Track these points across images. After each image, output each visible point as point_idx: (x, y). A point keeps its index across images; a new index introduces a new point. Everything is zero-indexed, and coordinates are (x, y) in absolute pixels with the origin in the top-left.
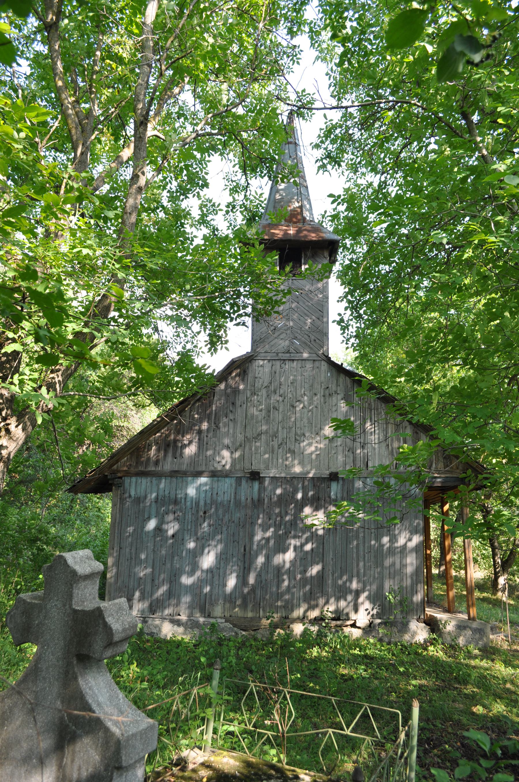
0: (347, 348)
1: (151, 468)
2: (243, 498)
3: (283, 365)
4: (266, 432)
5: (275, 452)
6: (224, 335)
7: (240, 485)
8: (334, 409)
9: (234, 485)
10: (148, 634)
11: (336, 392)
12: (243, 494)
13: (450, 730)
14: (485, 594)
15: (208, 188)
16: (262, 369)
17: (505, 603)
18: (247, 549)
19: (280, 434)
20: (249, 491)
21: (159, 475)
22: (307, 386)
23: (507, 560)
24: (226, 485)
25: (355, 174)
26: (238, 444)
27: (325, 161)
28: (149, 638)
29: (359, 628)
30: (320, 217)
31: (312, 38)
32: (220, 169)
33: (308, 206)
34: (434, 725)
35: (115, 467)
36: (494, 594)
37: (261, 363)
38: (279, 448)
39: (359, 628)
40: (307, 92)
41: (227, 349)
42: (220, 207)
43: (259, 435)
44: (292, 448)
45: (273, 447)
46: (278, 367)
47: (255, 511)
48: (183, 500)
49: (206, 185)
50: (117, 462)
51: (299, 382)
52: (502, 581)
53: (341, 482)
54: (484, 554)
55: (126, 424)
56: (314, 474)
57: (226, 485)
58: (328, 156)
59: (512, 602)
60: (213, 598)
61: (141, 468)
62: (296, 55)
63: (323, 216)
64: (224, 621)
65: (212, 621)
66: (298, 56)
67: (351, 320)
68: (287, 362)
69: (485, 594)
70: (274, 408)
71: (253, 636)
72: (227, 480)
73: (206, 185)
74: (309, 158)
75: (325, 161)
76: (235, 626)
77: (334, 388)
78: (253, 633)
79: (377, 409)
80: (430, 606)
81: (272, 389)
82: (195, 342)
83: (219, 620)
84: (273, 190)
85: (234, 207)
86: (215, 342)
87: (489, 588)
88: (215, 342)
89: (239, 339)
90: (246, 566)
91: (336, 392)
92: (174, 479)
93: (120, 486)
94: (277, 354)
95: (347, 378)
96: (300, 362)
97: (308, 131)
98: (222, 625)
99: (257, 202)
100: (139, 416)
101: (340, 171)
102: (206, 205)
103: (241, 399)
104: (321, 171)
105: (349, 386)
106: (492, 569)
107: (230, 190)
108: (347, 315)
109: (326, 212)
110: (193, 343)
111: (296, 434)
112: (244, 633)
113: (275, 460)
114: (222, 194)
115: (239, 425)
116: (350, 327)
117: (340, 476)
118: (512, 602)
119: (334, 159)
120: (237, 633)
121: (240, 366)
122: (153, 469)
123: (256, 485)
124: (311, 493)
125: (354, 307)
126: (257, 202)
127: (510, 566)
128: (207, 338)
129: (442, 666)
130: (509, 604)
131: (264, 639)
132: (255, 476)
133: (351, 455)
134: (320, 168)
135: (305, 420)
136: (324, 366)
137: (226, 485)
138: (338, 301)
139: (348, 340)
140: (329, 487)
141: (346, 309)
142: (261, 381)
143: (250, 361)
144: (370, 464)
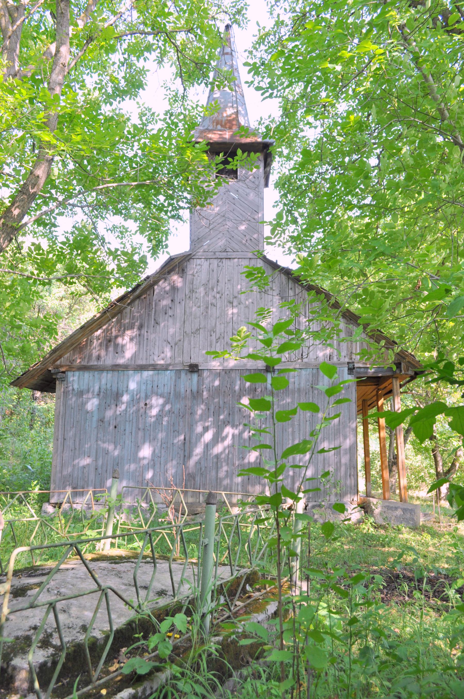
1: (94, 362)
2: (183, 391)
3: (220, 264)
7: (180, 378)
9: (174, 378)
12: (182, 386)
16: (199, 269)
24: (166, 378)
32: (160, 80)
35: (58, 362)
43: (198, 330)
45: (211, 342)
50: (60, 357)
68: (224, 260)
90: (186, 454)
92: (116, 373)
94: (215, 253)
105: (284, 283)
114: (159, 96)
115: (178, 320)
121: (176, 265)
122: (96, 363)
123: (195, 377)
132: (193, 368)
138: (274, 206)
143: (188, 260)
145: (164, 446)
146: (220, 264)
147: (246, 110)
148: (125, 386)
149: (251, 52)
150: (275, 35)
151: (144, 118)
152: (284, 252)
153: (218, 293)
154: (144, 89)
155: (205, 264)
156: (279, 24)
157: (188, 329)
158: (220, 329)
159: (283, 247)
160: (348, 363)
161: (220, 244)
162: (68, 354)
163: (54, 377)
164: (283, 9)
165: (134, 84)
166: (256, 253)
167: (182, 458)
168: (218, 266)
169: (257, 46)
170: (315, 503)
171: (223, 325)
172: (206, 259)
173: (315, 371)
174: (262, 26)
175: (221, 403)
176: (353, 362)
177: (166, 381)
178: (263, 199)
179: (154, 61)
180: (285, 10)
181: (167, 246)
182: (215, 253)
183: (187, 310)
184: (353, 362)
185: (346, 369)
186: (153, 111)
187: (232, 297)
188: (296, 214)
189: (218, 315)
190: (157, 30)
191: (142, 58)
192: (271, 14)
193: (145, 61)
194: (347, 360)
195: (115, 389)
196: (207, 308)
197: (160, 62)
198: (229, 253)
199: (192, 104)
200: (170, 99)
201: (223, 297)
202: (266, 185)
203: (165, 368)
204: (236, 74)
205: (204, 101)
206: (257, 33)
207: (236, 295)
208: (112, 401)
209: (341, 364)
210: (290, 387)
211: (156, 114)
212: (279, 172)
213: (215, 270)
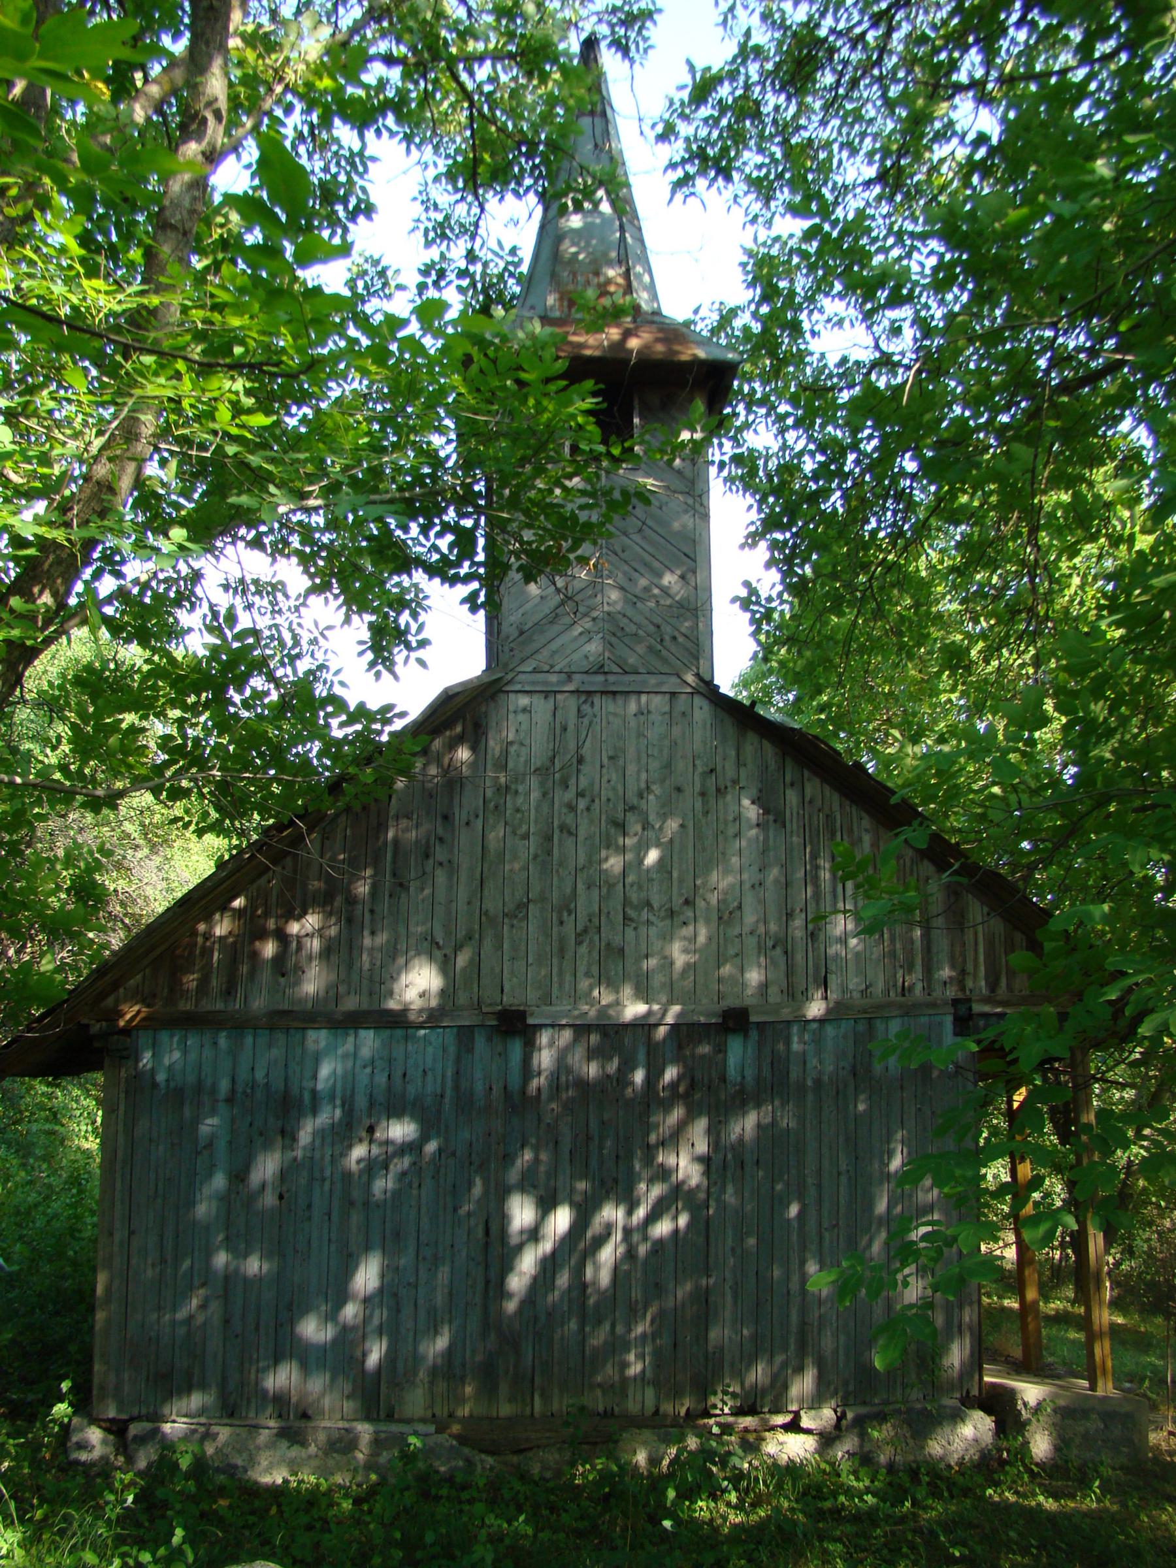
2: (479, 1087)
3: (586, 708)
4: (543, 899)
5: (569, 955)
6: (414, 627)
7: (471, 1050)
8: (731, 831)
9: (452, 1049)
12: (478, 1075)
15: (369, 217)
16: (523, 724)
18: (494, 1229)
19: (581, 901)
21: (239, 1025)
22: (654, 765)
25: (767, 204)
26: (461, 934)
27: (691, 169)
28: (221, 1478)
29: (808, 1431)
33: (646, 278)
37: (524, 701)
38: (579, 943)
39: (808, 1431)
41: (422, 663)
43: (523, 906)
44: (617, 940)
45: (562, 940)
46: (574, 710)
49: (366, 209)
51: (631, 752)
53: (754, 1035)
55: (122, 885)
58: (701, 155)
61: (185, 1006)
68: (597, 699)
70: (563, 828)
73: (366, 209)
74: (646, 165)
75: (691, 169)
77: (730, 773)
78: (515, 1459)
79: (851, 831)
81: (558, 771)
84: (549, 235)
85: (441, 274)
88: (386, 642)
89: (452, 642)
92: (281, 1037)
95: (766, 744)
100: (166, 862)
101: (728, 193)
103: (470, 801)
104: (679, 197)
105: (773, 765)
111: (626, 902)
112: (490, 1460)
113: (568, 977)
114: (407, 230)
117: (754, 1018)
119: (711, 162)
120: (469, 1462)
121: (459, 712)
122: (220, 1006)
123: (516, 1048)
124: (670, 1074)
128: (366, 635)
134: (679, 184)
136: (702, 711)
138: (742, 547)
140: (721, 1049)
142: (524, 751)
143: (493, 697)
144: (640, 505)
146: (586, 708)
151: (360, 284)
153: (580, 794)
155: (542, 708)
156: (747, 52)
157: (492, 904)
158: (586, 903)
160: (955, 1002)
162: (139, 977)
168: (580, 714)
170: (863, 1410)
173: (861, 1027)
175: (594, 1124)
176: (969, 1000)
178: (706, 517)
184: (969, 1000)
185: (948, 1020)
186: (383, 263)
187: (621, 807)
189: (582, 861)
194: (951, 992)
196: (549, 838)
198: (611, 678)
200: (427, 231)
204: (620, 171)
205: (525, 239)
207: (635, 801)
209: (934, 1005)
210: (793, 1076)
211: (389, 273)
213: (571, 727)
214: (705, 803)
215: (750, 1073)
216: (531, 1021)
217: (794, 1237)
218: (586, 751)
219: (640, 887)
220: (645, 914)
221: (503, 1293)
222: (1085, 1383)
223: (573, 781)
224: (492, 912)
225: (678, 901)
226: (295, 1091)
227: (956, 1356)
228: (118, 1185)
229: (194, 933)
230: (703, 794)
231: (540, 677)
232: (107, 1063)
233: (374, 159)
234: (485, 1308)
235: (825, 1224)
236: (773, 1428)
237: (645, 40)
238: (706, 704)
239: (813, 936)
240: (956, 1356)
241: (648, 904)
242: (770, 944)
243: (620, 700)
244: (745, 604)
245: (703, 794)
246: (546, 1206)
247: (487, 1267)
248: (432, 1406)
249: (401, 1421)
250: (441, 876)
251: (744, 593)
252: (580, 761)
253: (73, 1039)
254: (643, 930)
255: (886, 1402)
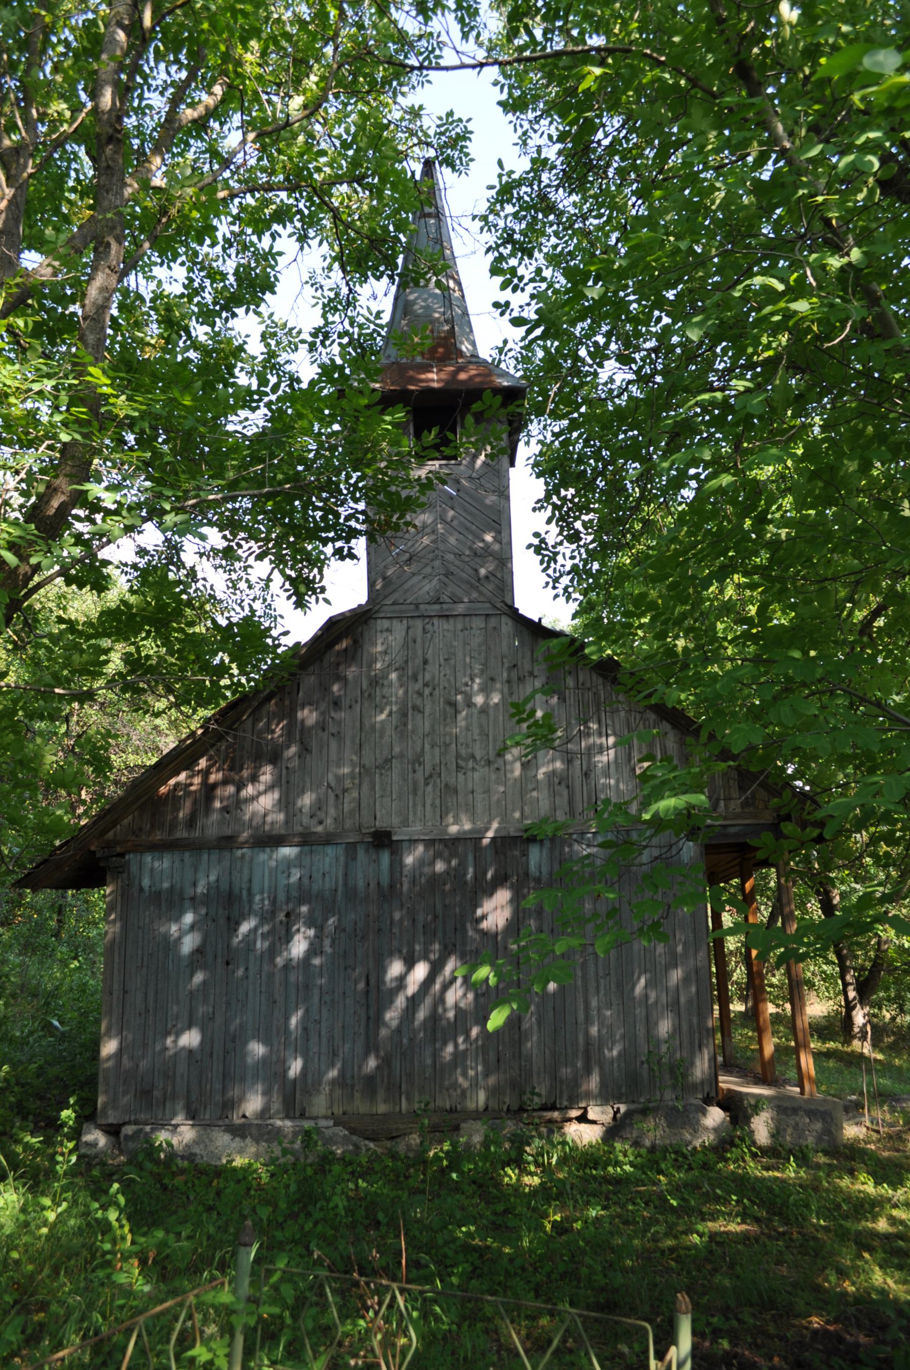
0: (556, 596)
1: (181, 833)
2: (361, 883)
4: (401, 755)
5: (420, 793)
7: (354, 859)
10: (183, 1157)
11: (531, 674)
12: (360, 875)
13: (772, 1329)
14: (831, 1045)
17: (868, 1059)
18: (372, 981)
19: (427, 757)
20: (371, 869)
21: (196, 847)
23: (867, 980)
24: (327, 860)
29: (594, 1122)
30: (495, 353)
31: (461, 21)
32: (303, 272)
34: (739, 1320)
35: (110, 835)
36: (848, 1041)
37: (386, 624)
38: (427, 784)
39: (594, 1122)
40: (456, 117)
41: (327, 601)
42: (302, 337)
43: (388, 761)
44: (452, 781)
45: (415, 783)
46: (420, 630)
47: (386, 906)
48: (245, 893)
50: (114, 824)
52: (859, 1017)
53: (547, 844)
54: (824, 972)
56: (496, 831)
57: (329, 859)
59: (880, 1057)
60: (309, 1081)
62: (433, 50)
63: (501, 350)
64: (331, 1123)
65: (307, 1125)
66: (437, 52)
67: (561, 543)
68: (435, 621)
69: (831, 1045)
70: (415, 708)
71: (390, 1150)
72: (329, 850)
76: (353, 1131)
77: (527, 667)
78: (388, 1144)
80: (729, 1072)
82: (269, 598)
83: (322, 1123)
84: (401, 306)
85: (326, 336)
86: (303, 590)
87: (837, 1034)
89: (346, 584)
90: (372, 1014)
91: (531, 674)
92: (227, 854)
93: (121, 870)
94: (417, 606)
96: (460, 619)
97: (464, 195)
98: (328, 1133)
99: (372, 327)
100: (151, 734)
102: (274, 334)
106: (841, 998)
107: (324, 306)
108: (553, 534)
109: (505, 342)
110: (265, 600)
111: (458, 756)
113: (419, 808)
114: (302, 304)
115: (348, 743)
116: (559, 558)
118: (880, 1057)
120: (357, 1147)
121: (342, 631)
122: (185, 835)
123: (385, 858)
125: (563, 519)
126: (372, 327)
127: (874, 992)
129: (754, 1189)
130: (876, 1060)
131: (411, 1155)
132: (382, 840)
133: (565, 792)
135: (476, 731)
136: (507, 626)
137: (327, 860)
138: (534, 510)
139: (556, 580)
140: (525, 854)
141: (549, 522)
143: (366, 622)
145: (327, 998)
146: (429, 627)
147: (459, 284)
148: (246, 878)
149: (484, 218)
150: (531, 185)
152: (556, 596)
153: (426, 685)
154: (274, 293)
156: (540, 164)
157: (368, 761)
159: (554, 588)
161: (426, 588)
163: (102, 864)
164: (545, 136)
165: (254, 286)
166: (499, 605)
167: (363, 1022)
168: (425, 631)
169: (498, 207)
171: (437, 750)
172: (401, 618)
174: (507, 169)
175: (439, 907)
177: (327, 865)
178: (508, 498)
179: (290, 236)
180: (550, 137)
181: (323, 590)
182: (417, 606)
183: (366, 723)
186: (289, 325)
188: (578, 525)
190: (296, 181)
191: (268, 234)
192: (525, 143)
193: (274, 239)
195: (224, 886)
196: (405, 715)
197: (303, 239)
198: (445, 606)
199: (367, 314)
201: (437, 692)
202: (512, 464)
203: (328, 840)
205: (386, 305)
206: (496, 182)
208: (221, 911)
212: (539, 442)
213: (419, 640)
214: (510, 688)
215: (545, 870)
216: (395, 838)
217: (579, 983)
218: (429, 656)
219: (467, 746)
220: (471, 764)
221: (378, 1020)
222: (798, 1089)
223: (420, 676)
224: (368, 765)
225: (492, 756)
226: (236, 890)
227: (701, 1067)
228: (116, 959)
229: (615, 734)
230: (509, 682)
231: (397, 607)
232: (108, 879)
233: (280, 254)
234: (367, 1035)
235: (601, 973)
236: (570, 1120)
237: (467, 155)
238: (510, 622)
239: (586, 775)
240: (701, 1067)
241: (473, 757)
242: (556, 781)
243: (452, 621)
244: (538, 550)
245: (509, 682)
246: (410, 965)
247: (368, 1008)
248: (331, 1107)
249: (310, 1118)
250: (334, 744)
251: (536, 541)
252: (425, 662)
253: (83, 863)
254: (470, 774)
255: (649, 1101)
